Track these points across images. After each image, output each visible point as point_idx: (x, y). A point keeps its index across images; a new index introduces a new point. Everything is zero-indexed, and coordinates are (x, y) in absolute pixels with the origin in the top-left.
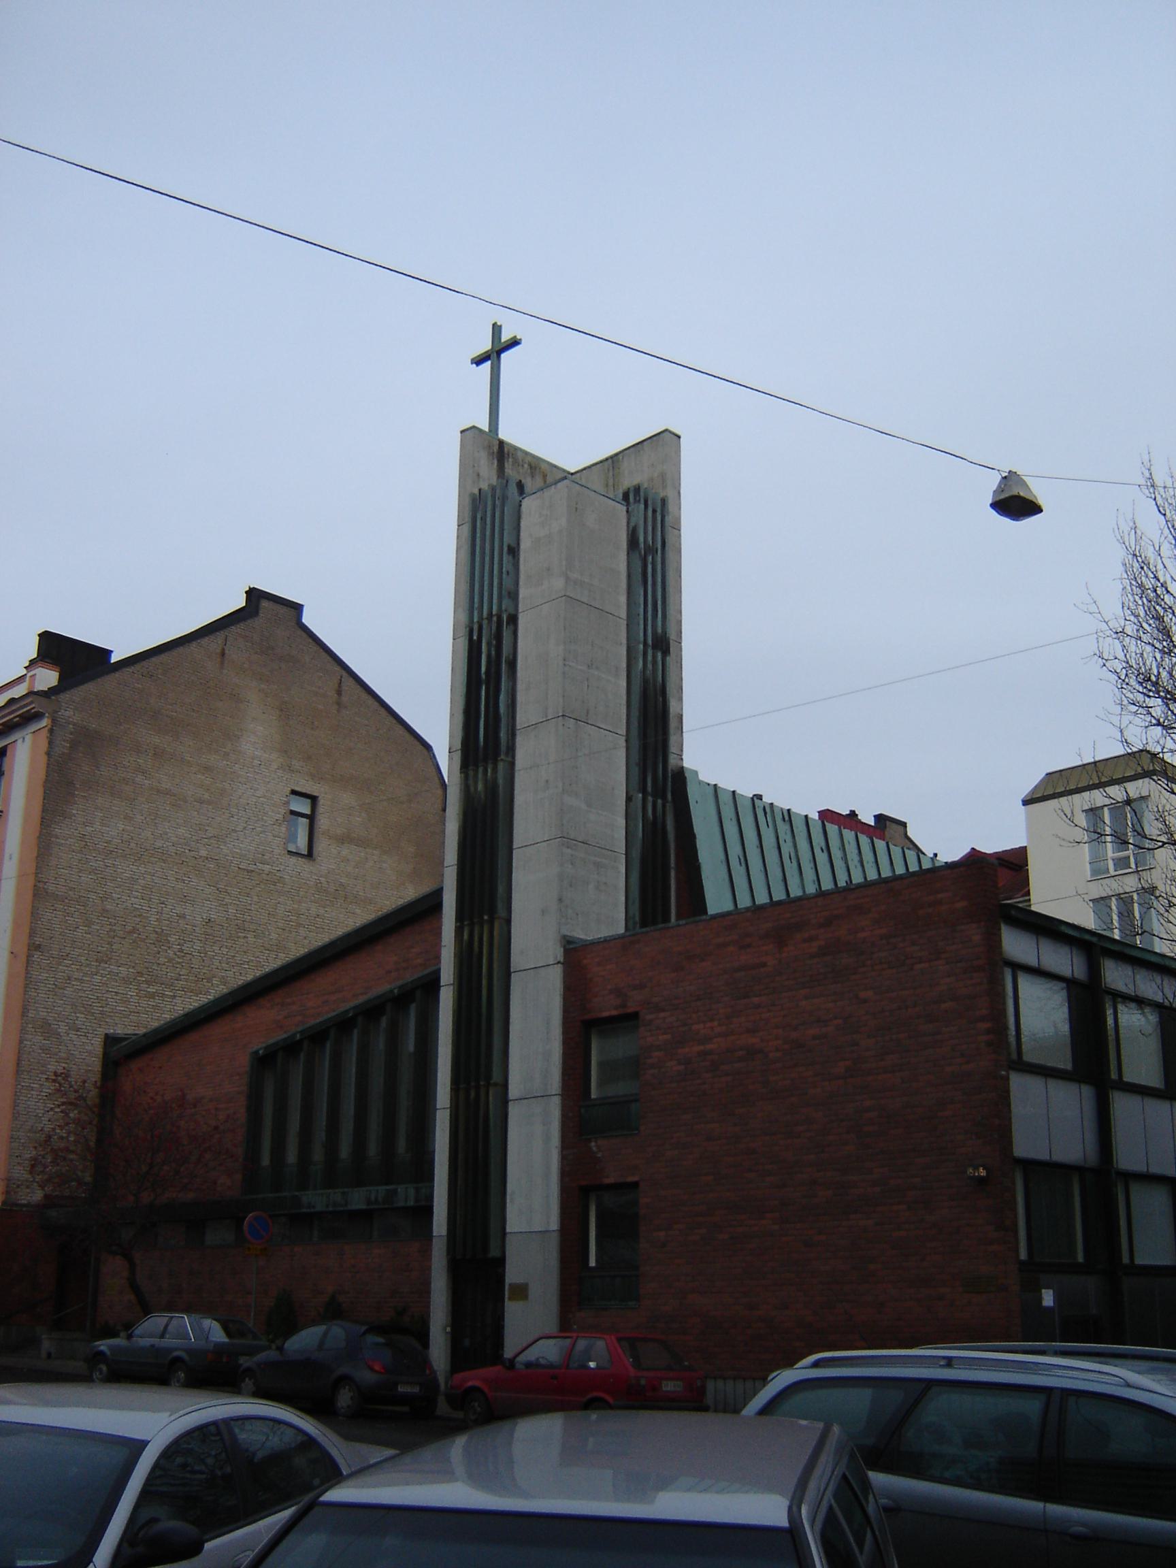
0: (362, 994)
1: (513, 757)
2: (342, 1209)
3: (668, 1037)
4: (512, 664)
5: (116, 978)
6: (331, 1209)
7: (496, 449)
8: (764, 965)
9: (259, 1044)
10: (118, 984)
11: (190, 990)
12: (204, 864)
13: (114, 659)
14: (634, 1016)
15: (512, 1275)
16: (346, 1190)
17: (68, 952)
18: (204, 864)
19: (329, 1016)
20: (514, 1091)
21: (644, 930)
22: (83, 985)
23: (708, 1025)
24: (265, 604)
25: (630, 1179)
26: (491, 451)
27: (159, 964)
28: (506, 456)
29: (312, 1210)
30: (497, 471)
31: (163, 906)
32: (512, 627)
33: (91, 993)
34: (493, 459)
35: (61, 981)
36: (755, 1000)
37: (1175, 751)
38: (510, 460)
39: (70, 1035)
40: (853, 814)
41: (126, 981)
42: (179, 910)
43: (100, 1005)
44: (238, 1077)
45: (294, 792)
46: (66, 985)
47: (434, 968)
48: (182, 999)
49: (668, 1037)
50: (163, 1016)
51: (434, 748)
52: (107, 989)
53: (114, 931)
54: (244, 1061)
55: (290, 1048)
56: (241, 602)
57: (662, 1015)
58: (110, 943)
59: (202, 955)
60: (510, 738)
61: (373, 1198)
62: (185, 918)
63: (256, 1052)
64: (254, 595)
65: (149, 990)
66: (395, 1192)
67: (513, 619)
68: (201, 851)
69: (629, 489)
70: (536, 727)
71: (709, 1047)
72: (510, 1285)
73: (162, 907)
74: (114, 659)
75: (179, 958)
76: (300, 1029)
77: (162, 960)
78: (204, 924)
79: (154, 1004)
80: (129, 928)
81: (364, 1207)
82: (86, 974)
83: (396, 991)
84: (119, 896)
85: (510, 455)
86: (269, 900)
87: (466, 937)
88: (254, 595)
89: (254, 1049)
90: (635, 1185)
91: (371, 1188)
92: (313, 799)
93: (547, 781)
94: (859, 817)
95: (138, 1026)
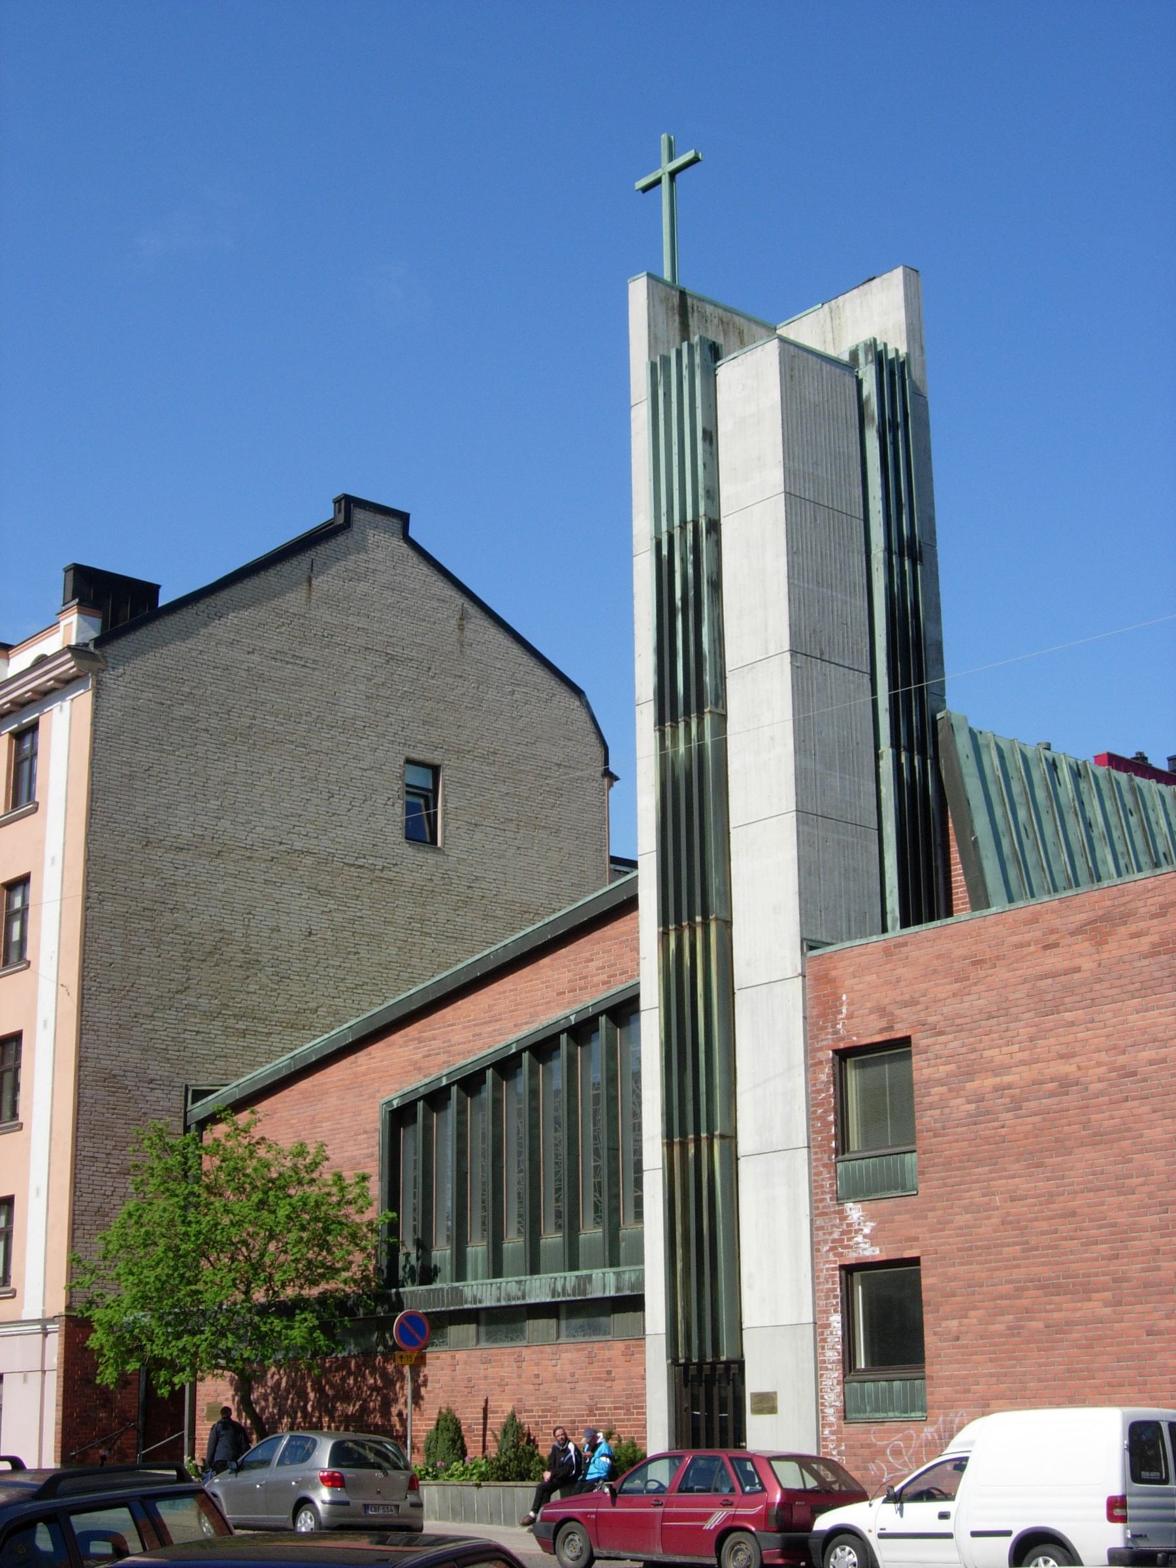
0: (526, 1023)
1: (725, 707)
2: (518, 1302)
3: (953, 1067)
4: (716, 585)
5: (196, 1012)
6: (503, 1303)
7: (676, 301)
8: (1078, 970)
9: (394, 1092)
10: (198, 1021)
11: (290, 1025)
12: (299, 859)
13: (163, 601)
14: (906, 1041)
15: (754, 1383)
16: (523, 1278)
17: (133, 981)
18: (299, 859)
19: (485, 1053)
20: (746, 1143)
21: (977, 913)
22: (153, 1023)
23: (1005, 1049)
24: (359, 515)
25: (908, 1254)
26: (671, 305)
27: (248, 993)
28: (690, 309)
29: (479, 1306)
30: (680, 330)
31: (251, 916)
32: (714, 536)
33: (165, 1033)
34: (674, 314)
35: (126, 1019)
36: (1068, 1016)
37: (1173, 1203)
38: (696, 314)
39: (141, 1089)
40: (1141, 758)
41: (210, 1016)
42: (272, 923)
43: (176, 1048)
44: (364, 1136)
45: (409, 761)
46: (132, 1024)
47: (633, 982)
48: (281, 1037)
49: (953, 1067)
50: (258, 1059)
51: (586, 693)
52: (185, 1027)
53: (191, 952)
54: (374, 1120)
55: (436, 1098)
56: (324, 513)
57: (941, 1039)
58: (187, 969)
59: (302, 978)
60: (719, 681)
61: (560, 1289)
62: (279, 931)
63: (389, 1103)
64: (348, 504)
65: (237, 1026)
66: (589, 1277)
67: (714, 526)
68: (295, 843)
69: (857, 346)
70: (753, 668)
71: (1007, 1079)
72: (753, 1395)
73: (249, 919)
74: (163, 601)
75: (272, 983)
76: (446, 1071)
77: (252, 988)
78: (303, 937)
79: (245, 1044)
80: (208, 949)
81: (548, 1300)
82: (157, 1009)
83: (572, 1018)
84: (194, 907)
85: (695, 308)
86: (384, 903)
87: (672, 946)
88: (348, 504)
89: (386, 1099)
90: (916, 1261)
91: (555, 1275)
92: (435, 770)
93: (772, 738)
94: (1150, 761)
95: (226, 1074)
